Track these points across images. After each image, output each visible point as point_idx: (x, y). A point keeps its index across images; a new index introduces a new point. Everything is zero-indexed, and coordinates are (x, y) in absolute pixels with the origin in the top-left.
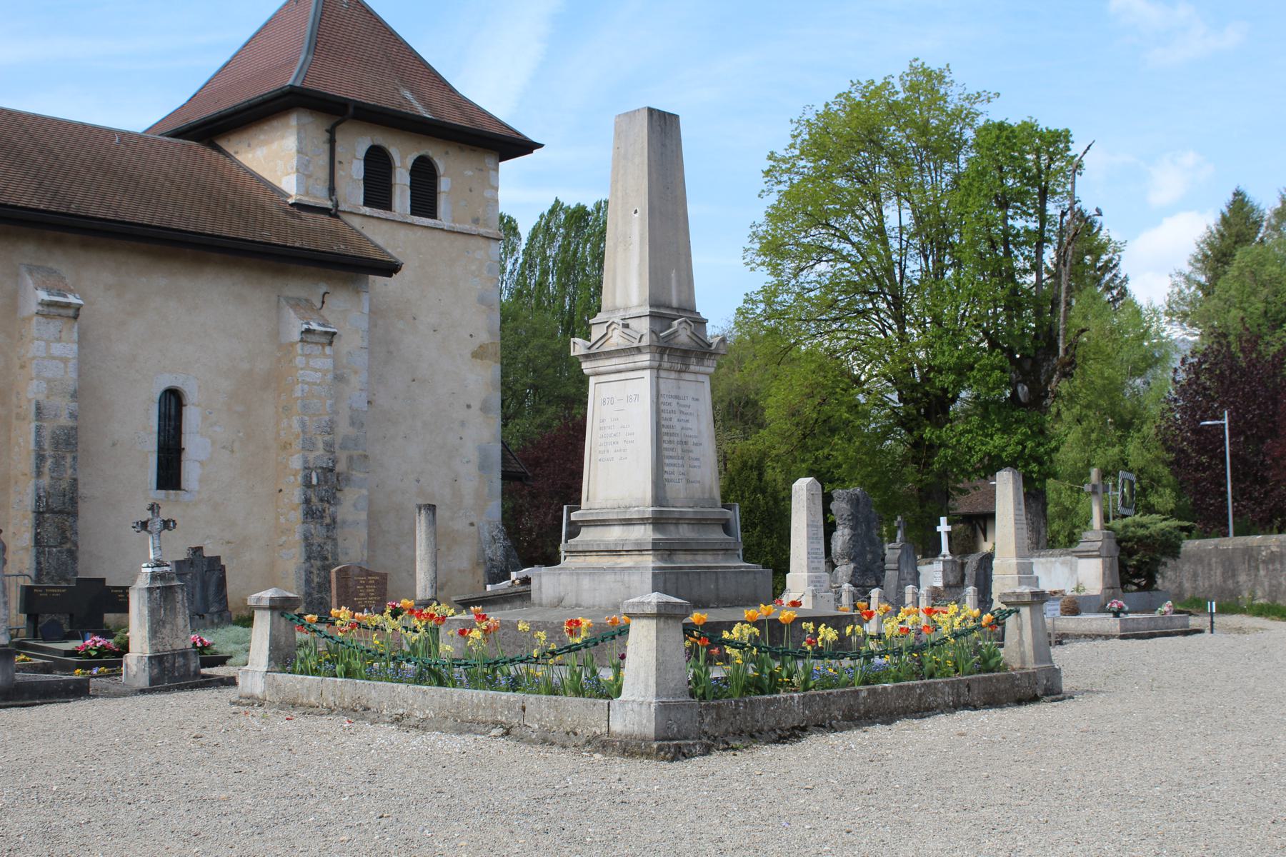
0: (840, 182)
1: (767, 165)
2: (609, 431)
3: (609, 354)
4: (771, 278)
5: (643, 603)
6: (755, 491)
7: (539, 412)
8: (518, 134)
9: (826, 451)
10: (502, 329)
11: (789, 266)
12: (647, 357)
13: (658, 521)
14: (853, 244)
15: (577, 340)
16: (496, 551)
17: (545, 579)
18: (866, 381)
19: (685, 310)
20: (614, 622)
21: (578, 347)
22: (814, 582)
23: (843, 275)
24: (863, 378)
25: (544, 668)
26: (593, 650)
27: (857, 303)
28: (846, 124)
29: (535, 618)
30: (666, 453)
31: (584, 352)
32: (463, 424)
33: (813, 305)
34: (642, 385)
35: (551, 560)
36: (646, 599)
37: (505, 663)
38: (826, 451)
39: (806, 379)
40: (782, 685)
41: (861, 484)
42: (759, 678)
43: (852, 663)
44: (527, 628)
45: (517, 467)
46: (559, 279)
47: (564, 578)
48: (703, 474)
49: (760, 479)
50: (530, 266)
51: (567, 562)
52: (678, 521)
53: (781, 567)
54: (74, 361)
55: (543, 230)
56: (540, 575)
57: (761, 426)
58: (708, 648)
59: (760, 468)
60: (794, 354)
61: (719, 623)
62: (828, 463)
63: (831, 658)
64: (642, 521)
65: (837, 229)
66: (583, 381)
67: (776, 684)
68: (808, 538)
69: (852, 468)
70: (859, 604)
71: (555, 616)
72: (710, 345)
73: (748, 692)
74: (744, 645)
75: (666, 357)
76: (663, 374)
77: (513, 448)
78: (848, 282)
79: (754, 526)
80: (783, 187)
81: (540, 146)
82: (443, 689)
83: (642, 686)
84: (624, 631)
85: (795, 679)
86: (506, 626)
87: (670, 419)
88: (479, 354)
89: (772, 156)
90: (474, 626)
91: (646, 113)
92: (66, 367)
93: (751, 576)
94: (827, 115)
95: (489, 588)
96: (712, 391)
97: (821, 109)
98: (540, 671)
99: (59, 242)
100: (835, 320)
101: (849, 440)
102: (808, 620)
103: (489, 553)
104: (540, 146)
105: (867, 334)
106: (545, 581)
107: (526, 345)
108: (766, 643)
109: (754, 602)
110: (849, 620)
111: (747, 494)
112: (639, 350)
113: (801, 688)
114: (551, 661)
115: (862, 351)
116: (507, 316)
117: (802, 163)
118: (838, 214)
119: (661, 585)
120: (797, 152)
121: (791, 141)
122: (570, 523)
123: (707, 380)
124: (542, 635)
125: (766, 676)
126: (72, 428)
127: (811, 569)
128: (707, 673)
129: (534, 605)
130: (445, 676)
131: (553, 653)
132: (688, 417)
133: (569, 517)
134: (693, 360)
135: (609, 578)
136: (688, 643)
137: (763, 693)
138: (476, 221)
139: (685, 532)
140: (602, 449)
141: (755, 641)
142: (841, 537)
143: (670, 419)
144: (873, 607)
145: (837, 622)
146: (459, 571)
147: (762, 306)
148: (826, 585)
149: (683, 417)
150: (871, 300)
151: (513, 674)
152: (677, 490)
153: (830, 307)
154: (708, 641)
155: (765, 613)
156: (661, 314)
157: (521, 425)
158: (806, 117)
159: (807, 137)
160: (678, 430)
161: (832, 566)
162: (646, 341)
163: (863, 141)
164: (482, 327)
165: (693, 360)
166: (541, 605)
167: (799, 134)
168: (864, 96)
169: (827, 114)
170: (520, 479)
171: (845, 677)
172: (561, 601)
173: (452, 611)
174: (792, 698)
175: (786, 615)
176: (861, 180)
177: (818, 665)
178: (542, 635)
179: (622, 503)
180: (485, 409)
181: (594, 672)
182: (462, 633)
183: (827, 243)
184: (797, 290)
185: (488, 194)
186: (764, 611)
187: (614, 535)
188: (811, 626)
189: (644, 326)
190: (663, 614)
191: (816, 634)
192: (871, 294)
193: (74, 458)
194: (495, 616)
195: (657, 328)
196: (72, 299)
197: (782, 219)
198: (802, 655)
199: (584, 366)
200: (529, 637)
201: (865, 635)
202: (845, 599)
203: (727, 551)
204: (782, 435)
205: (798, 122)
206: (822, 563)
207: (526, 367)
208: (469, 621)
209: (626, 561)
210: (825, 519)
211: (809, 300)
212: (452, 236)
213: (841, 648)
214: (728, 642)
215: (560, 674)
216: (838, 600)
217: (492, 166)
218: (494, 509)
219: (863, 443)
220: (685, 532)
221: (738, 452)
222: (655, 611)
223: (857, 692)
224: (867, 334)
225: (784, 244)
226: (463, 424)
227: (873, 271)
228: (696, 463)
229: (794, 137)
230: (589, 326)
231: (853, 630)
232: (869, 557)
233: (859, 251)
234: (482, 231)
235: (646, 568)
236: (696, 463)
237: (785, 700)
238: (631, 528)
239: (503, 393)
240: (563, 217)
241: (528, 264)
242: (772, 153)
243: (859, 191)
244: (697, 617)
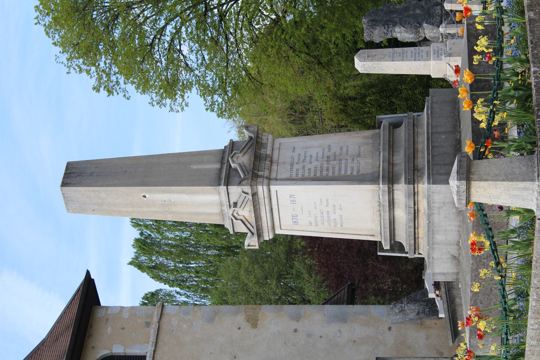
0: (117, 34)
1: (103, 93)
2: (319, 219)
3: (258, 218)
4: (194, 90)
5: (458, 192)
6: (364, 103)
7: (298, 276)
8: (78, 290)
9: (331, 46)
10: (234, 304)
11: (184, 75)
12: (260, 188)
13: (391, 180)
14: (167, 24)
15: (246, 243)
16: (412, 309)
17: (437, 270)
18: (276, 15)
19: (223, 158)
20: (472, 215)
21: (251, 243)
22: (438, 55)
23: (191, 33)
24: (274, 17)
25: (509, 271)
26: (495, 232)
27: (214, 21)
28: (71, 30)
29: (468, 278)
30: (336, 173)
31: (255, 238)
32: (309, 335)
33: (215, 57)
34: (282, 192)
35: (419, 265)
36: (454, 190)
37: (505, 302)
38: (331, 46)
39: (274, 62)
40: (524, 81)
41: (359, 18)
42: (518, 99)
43: (506, 24)
44: (477, 285)
45: (344, 293)
46: (193, 259)
47: (436, 254)
48: (353, 144)
49: (354, 99)
50: (183, 281)
51: (423, 252)
52: (391, 164)
53: (425, 82)
55: (154, 271)
56: (434, 274)
57: (311, 98)
58: (494, 139)
59: (345, 99)
60: (253, 72)
61: (473, 131)
62: (341, 45)
63: (502, 41)
64: (391, 192)
65: (155, 37)
66: (276, 239)
67: (524, 85)
68: (403, 60)
69: (345, 25)
70: (457, 19)
71: (467, 263)
72: (251, 138)
73: (530, 107)
74: (491, 111)
75: (260, 173)
76: (273, 175)
77: (327, 296)
78: (197, 28)
79: (391, 103)
80: (122, 80)
81: (88, 273)
82: (527, 353)
83: (525, 193)
84: (480, 207)
85: (519, 70)
86: (475, 301)
87: (310, 169)
88: (254, 322)
89: (97, 89)
90: (475, 327)
91: (66, 189)
93: (435, 106)
94: (64, 44)
95: (441, 315)
96: (284, 137)
97: (59, 49)
98: (512, 274)
100: (227, 39)
101: (323, 27)
102: (471, 60)
103: (412, 315)
104: (88, 273)
105: (238, 14)
106: (438, 269)
107: (246, 285)
108: (490, 94)
109: (456, 103)
110: (471, 27)
111: (367, 110)
112: (255, 195)
113: (527, 65)
114: (504, 265)
115: (252, 17)
116: (222, 300)
117: (102, 64)
118: (143, 35)
119: (442, 177)
120: (93, 69)
121: (84, 74)
122: (392, 249)
123: (278, 141)
124: (483, 272)
125: (517, 94)
127: (428, 58)
128: (514, 141)
129: (457, 279)
130: (515, 351)
131: (498, 264)
133: (387, 251)
134: (263, 151)
135: (436, 219)
136: (490, 156)
137: (531, 96)
138: (148, 324)
139: (400, 158)
140: (332, 224)
141: (488, 102)
142: (402, 34)
143: (310, 169)
144: (462, 8)
145: (473, 37)
146: (427, 339)
147: (216, 97)
148: (440, 45)
149: (308, 159)
150: (212, 10)
151: (514, 296)
152: (366, 164)
153: (217, 42)
154: (488, 140)
155: (465, 94)
156: (226, 177)
157: (310, 291)
158: (65, 61)
159: (81, 60)
160: (318, 164)
161: (425, 41)
162: (248, 189)
163: (84, 16)
164: (231, 321)
165: (263, 151)
166: (458, 274)
167: (79, 67)
168: (48, 14)
169: (62, 45)
170: (354, 290)
171: (518, 30)
172: (454, 258)
173: (462, 344)
174: (535, 72)
175: (467, 77)
176: (116, 17)
177: (508, 52)
178: (483, 272)
179: (377, 208)
180: (297, 318)
181: (513, 231)
182: (481, 337)
183: (166, 45)
184: (203, 69)
185: (126, 315)
186: (463, 95)
187: (401, 215)
188: (476, 57)
189: (235, 191)
190: (467, 176)
191: (482, 53)
192: (206, 10)
194: (467, 310)
195: (237, 180)
197: (147, 81)
198: (499, 63)
199: (267, 238)
200: (485, 282)
201: (483, 14)
202: (452, 30)
203: (415, 125)
204: (318, 81)
205: (69, 67)
206: (424, 49)
207: (262, 285)
208: (471, 331)
209: (423, 205)
210: (386, 47)
211: (211, 59)
212: (160, 343)
213: (494, 33)
214: (489, 124)
215: (514, 258)
216: (453, 36)
217: (104, 311)
218: (377, 310)
219: (325, 17)
220: (400, 158)
221: (333, 117)
222: (464, 182)
223: (530, 20)
224: (238, 14)
225: (167, 79)
226: (309, 335)
227: (189, 8)
228: (344, 149)
229: (81, 71)
230: (236, 234)
231: (479, 23)
232: (418, 11)
233: (172, 20)
234: (155, 319)
235: (429, 189)
236: (344, 149)
237: (536, 78)
238: (396, 201)
239: (283, 303)
240: (143, 258)
241: (180, 283)
242: (94, 88)
243: (124, 20)
244: (468, 148)
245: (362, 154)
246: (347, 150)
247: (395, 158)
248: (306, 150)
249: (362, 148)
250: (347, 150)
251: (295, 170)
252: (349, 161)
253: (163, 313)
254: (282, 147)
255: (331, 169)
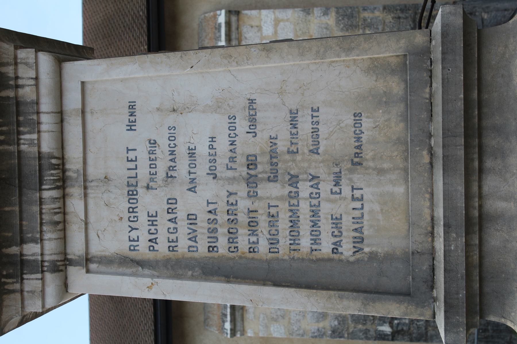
54: (277, 12)
75: (31, 250)
76: (76, 247)
92: (283, 20)
99: (175, 19)
126: (337, 13)
132: (182, 151)
143: (192, 218)
193: (364, 10)
196: (222, 19)
228: (305, 126)
245: (368, 153)
246: (315, 131)
247: (490, 183)
248: (171, 119)
249: (366, 123)
250: (315, 131)
251: (143, 218)
252: (326, 187)
253: (59, 78)
254: (92, 103)
255: (263, 220)
